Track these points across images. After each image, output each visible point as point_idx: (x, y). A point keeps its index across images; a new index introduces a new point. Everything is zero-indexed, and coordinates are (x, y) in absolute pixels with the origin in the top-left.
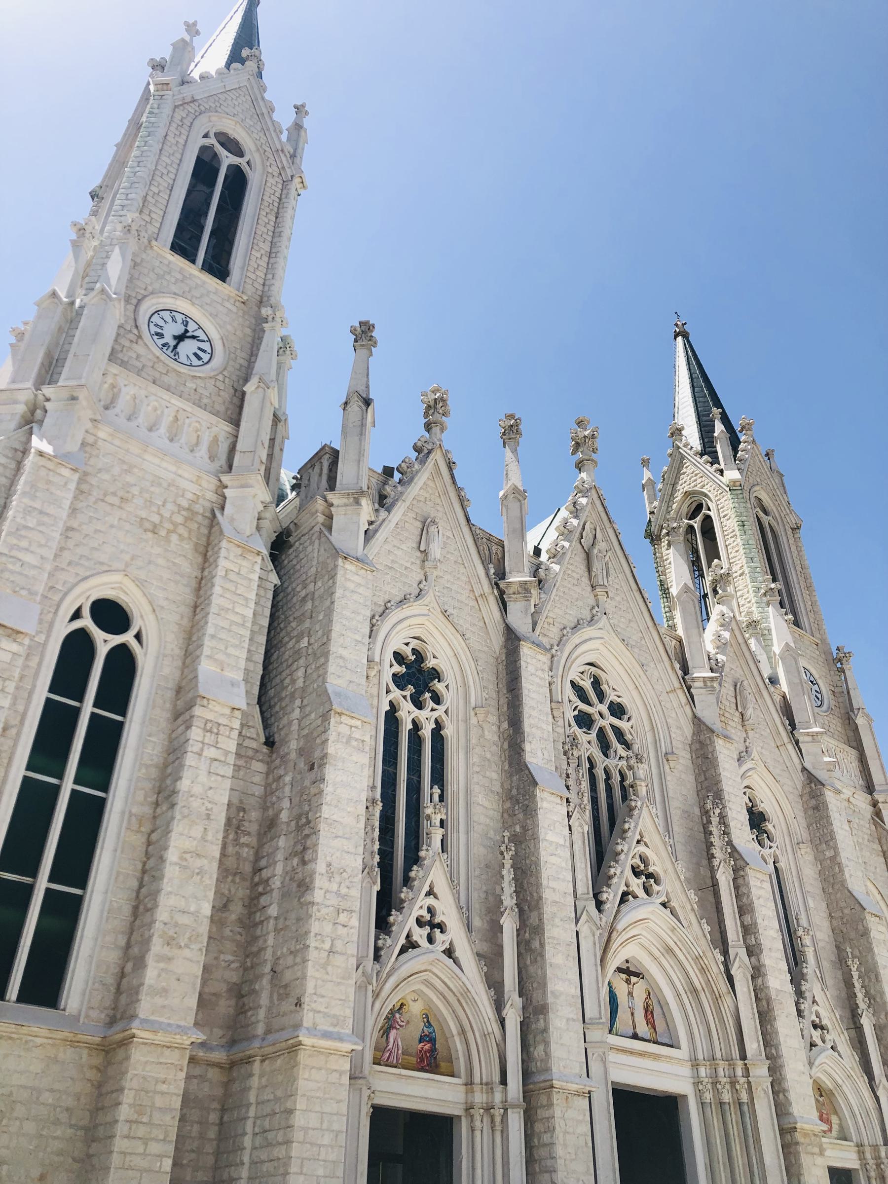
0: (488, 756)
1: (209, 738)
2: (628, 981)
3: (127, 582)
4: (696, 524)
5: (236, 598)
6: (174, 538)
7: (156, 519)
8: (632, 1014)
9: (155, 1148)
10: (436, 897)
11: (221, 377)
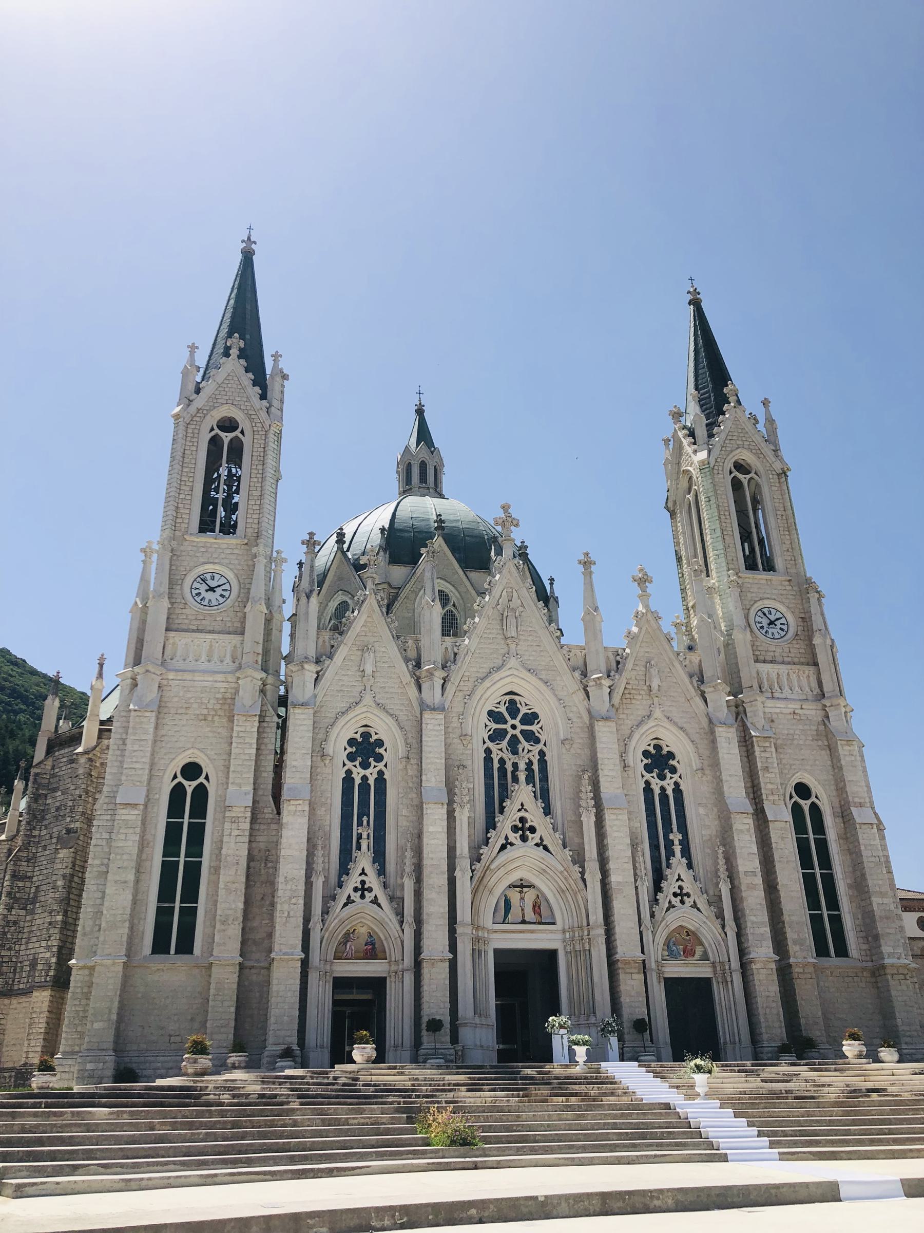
0: (411, 785)
1: (234, 826)
2: (521, 892)
3: (196, 751)
4: (690, 497)
5: (244, 746)
6: (216, 718)
7: (205, 712)
8: (523, 910)
9: (226, 1004)
10: (366, 875)
11: (237, 604)
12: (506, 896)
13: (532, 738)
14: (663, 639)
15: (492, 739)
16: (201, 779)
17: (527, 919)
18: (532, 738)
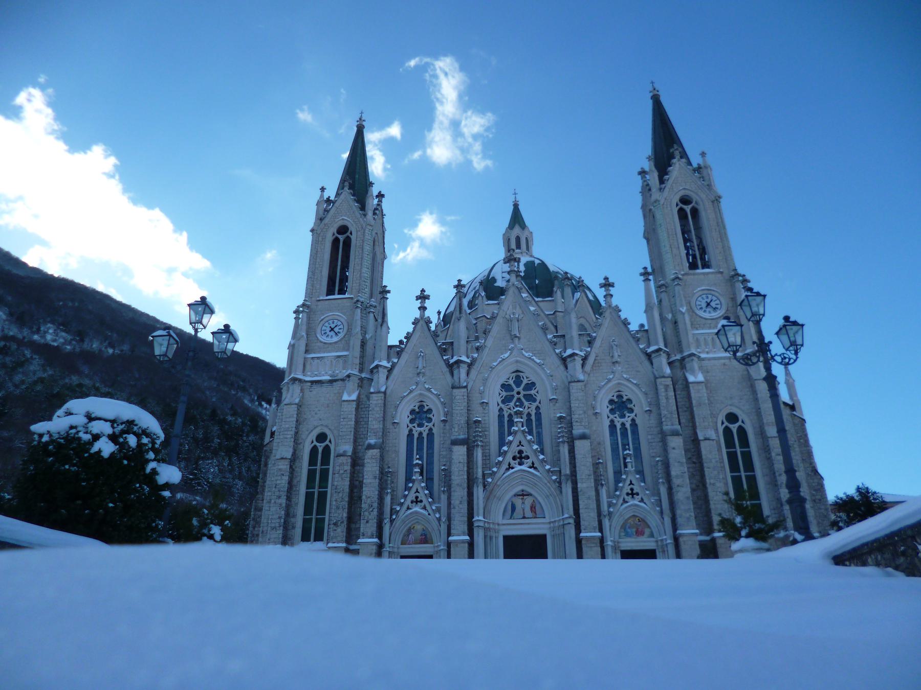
13: (531, 398)
14: (620, 323)
15: (503, 402)
16: (327, 442)
17: (526, 516)
18: (531, 398)
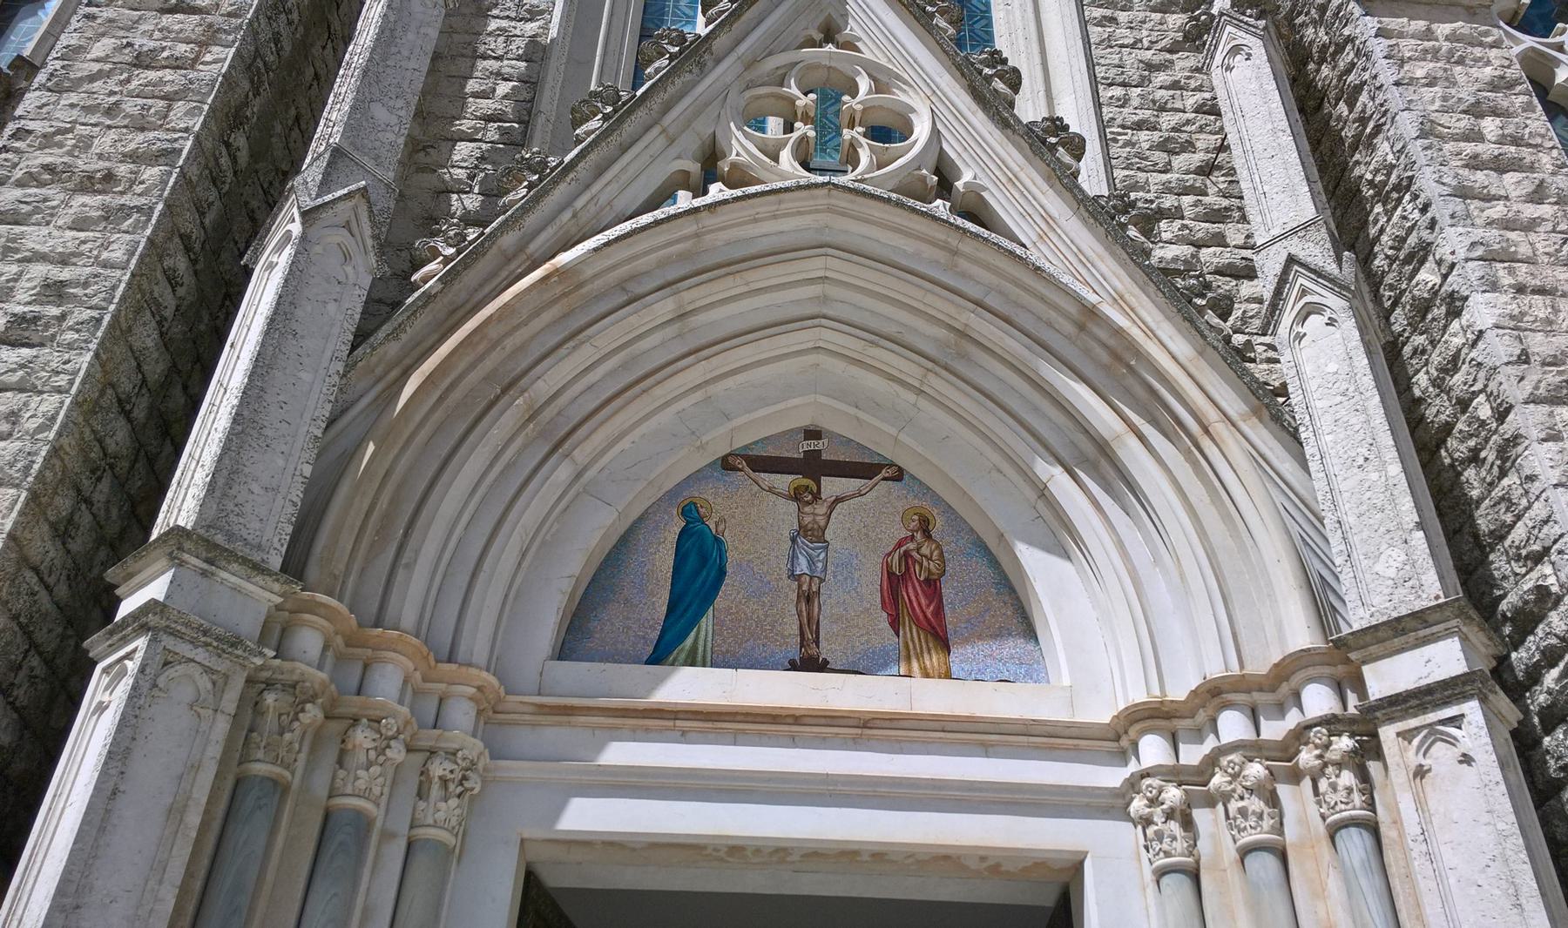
12: (691, 513)
